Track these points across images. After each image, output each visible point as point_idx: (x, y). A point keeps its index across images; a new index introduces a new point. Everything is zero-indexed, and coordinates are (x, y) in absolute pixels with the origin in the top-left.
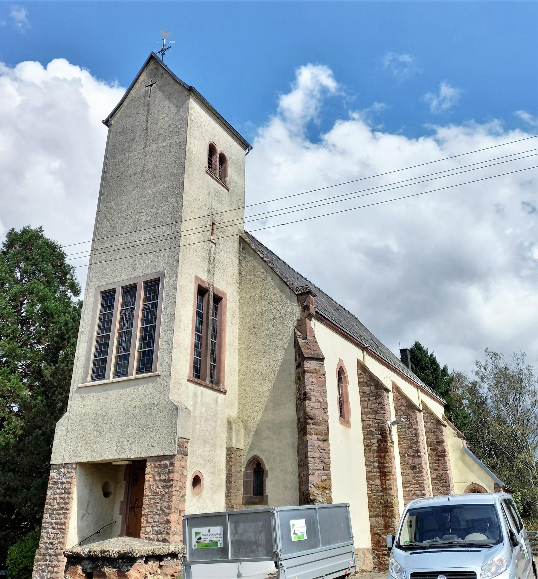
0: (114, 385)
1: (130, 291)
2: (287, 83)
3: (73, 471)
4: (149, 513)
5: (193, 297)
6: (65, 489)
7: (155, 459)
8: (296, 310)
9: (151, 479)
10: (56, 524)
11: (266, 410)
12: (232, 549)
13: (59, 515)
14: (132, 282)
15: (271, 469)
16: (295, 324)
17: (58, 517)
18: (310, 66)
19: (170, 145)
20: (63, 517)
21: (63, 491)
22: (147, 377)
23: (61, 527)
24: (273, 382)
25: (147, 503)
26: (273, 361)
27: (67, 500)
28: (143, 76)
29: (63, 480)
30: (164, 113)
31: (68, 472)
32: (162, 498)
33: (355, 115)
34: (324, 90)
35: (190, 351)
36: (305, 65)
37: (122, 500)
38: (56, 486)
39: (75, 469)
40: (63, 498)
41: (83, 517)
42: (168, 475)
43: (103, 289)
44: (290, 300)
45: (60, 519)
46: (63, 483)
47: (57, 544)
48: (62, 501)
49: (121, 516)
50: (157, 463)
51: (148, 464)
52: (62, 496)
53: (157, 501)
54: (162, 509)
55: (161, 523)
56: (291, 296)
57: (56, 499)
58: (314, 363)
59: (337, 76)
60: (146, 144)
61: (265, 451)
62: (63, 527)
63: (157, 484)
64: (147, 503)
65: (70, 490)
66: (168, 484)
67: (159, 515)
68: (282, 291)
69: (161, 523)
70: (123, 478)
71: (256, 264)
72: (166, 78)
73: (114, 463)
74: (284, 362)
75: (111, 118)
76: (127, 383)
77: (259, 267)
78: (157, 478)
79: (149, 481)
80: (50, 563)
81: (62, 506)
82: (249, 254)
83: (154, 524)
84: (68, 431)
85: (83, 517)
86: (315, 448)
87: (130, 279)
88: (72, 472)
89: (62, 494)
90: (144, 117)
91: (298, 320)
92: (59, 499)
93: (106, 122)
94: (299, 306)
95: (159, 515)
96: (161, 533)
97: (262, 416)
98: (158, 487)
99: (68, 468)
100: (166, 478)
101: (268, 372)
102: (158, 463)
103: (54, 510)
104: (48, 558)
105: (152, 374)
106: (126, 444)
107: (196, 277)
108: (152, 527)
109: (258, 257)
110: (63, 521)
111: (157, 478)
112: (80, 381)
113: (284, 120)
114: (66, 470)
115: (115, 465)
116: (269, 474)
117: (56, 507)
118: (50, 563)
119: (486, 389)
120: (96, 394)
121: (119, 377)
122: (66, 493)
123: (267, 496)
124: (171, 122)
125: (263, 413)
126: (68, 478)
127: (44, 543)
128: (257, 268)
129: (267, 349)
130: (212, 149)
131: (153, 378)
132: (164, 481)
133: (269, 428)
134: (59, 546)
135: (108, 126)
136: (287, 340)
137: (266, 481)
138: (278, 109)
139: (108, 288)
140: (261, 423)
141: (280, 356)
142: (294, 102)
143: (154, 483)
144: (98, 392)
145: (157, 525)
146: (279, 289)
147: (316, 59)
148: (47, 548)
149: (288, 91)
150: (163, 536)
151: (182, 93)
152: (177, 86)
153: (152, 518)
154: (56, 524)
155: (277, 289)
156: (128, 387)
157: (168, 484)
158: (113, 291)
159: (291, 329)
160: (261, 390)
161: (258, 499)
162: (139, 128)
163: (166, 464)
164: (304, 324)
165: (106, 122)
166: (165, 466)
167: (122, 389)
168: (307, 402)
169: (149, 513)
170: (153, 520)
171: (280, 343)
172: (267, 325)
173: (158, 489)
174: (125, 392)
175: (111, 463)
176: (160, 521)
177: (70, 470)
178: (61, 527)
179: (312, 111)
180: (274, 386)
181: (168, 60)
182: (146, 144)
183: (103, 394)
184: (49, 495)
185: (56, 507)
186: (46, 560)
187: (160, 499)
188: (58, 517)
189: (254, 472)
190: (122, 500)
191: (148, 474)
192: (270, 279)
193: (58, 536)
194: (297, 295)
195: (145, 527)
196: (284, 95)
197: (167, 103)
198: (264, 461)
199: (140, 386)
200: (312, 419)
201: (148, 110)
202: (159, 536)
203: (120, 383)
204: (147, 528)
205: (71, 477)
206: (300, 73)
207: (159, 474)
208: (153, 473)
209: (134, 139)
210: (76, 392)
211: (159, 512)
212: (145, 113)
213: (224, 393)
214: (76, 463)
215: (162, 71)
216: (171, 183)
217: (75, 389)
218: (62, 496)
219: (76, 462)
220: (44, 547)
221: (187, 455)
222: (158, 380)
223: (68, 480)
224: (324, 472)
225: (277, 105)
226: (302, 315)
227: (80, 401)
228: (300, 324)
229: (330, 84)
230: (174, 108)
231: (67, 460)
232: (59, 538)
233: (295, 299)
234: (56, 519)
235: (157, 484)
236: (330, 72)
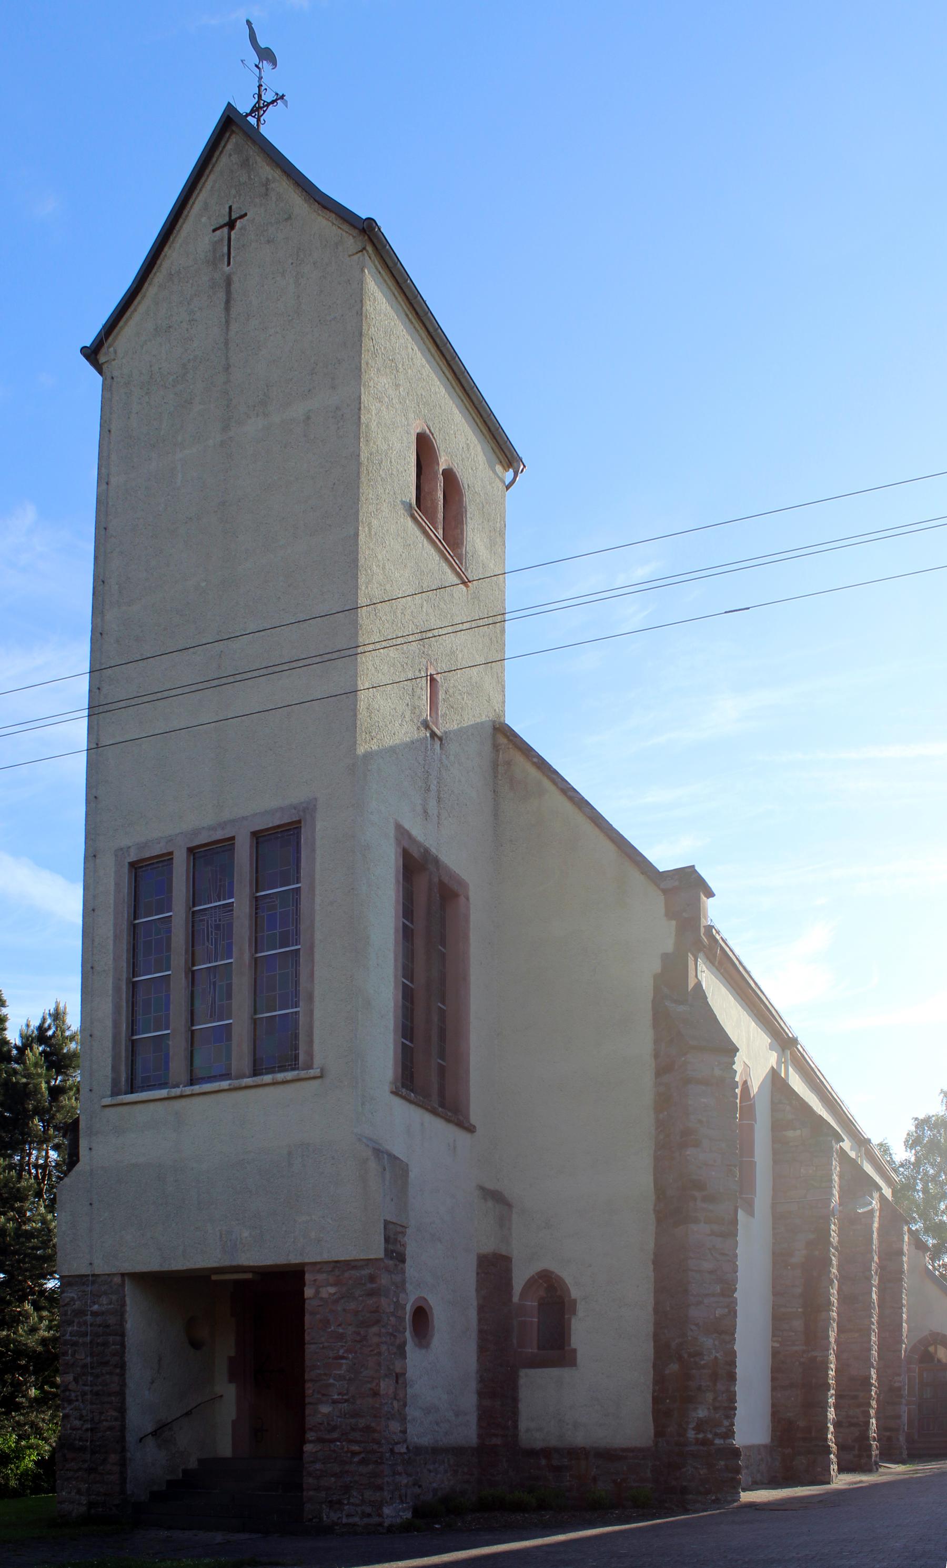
1: (210, 856)
5: (393, 880)
12: (647, 1526)
14: (219, 835)
35: (392, 1022)
41: (152, 1382)
51: (308, 1277)
73: (214, 1277)
85: (152, 1382)
87: (213, 828)
91: (665, 957)
93: (92, 354)
107: (399, 828)
115: (215, 1281)
116: (581, 1308)
119: (46, 1334)
123: (575, 1351)
130: (425, 448)
135: (99, 368)
137: (573, 1321)
158: (166, 859)
165: (92, 354)
168: (690, 1151)
181: (272, 127)
189: (540, 1305)
194: (664, 891)
213: (471, 1129)
214: (123, 1275)
219: (123, 1271)
221: (403, 1261)
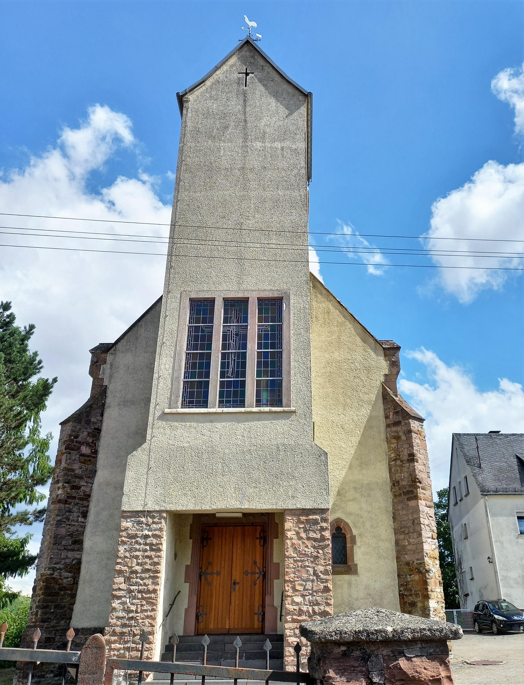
0: (224, 416)
2: (78, 119)
3: (163, 521)
4: (296, 579)
6: (151, 545)
7: (297, 512)
8: (382, 365)
9: (295, 537)
10: (139, 592)
11: (350, 467)
13: (142, 579)
15: (360, 535)
16: (382, 379)
17: (141, 582)
18: (107, 109)
19: (282, 149)
20: (150, 583)
21: (148, 548)
22: (254, 412)
23: (148, 595)
24: (358, 439)
25: (291, 566)
26: (357, 415)
27: (156, 560)
28: (233, 60)
29: (146, 532)
30: (268, 110)
31: (153, 523)
32: (315, 560)
33: (145, 177)
34: (117, 139)
36: (102, 106)
37: (189, 563)
38: (133, 541)
39: (165, 518)
40: (150, 557)
42: (320, 533)
43: (194, 295)
44: (375, 352)
45: (145, 584)
46: (146, 537)
47: (143, 619)
48: (147, 560)
49: (188, 585)
50: (303, 518)
52: (146, 554)
53: (307, 564)
54: (315, 574)
55: (316, 592)
56: (376, 348)
57: (137, 557)
58: (417, 423)
59: (135, 131)
60: (245, 140)
61: (351, 514)
62: (153, 595)
63: (303, 543)
64: (291, 566)
65: (160, 546)
66: (321, 544)
67: (313, 581)
68: (364, 341)
69: (316, 592)
70: (188, 535)
71: (330, 306)
72: (268, 72)
73: (217, 515)
74: (371, 418)
75: (190, 91)
76: (245, 416)
77: (334, 311)
78: (303, 535)
79: (291, 539)
80: (134, 645)
81: (148, 567)
82: (321, 294)
83: (305, 593)
84: (149, 469)
86: (424, 514)
87: (235, 291)
88: (161, 523)
89: (145, 551)
90: (239, 107)
91: (386, 375)
92: (141, 557)
94: (386, 361)
95: (313, 581)
96: (318, 604)
97: (346, 475)
98: (307, 547)
99: (153, 517)
100: (318, 536)
101: (352, 426)
102: (304, 518)
103: (133, 572)
104: (127, 638)
105: (242, 410)
106: (251, 491)
108: (303, 596)
109: (334, 300)
110: (151, 587)
111: (303, 535)
112: (166, 405)
113: (65, 155)
114: (150, 520)
117: (138, 568)
118: (134, 645)
120: (194, 424)
121: (237, 407)
122: (152, 550)
124: (281, 123)
125: (347, 472)
126: (155, 530)
127: (118, 618)
128: (332, 311)
129: (348, 401)
131: (285, 414)
132: (315, 540)
133: (355, 489)
134: (147, 621)
136: (373, 394)
138: (59, 141)
139: (202, 295)
140: (344, 483)
141: (365, 411)
142: (80, 141)
143: (300, 542)
144: (196, 422)
145: (310, 594)
146: (361, 339)
147: (116, 105)
148: (124, 626)
149: (75, 126)
150: (322, 608)
151: (293, 96)
152: (286, 86)
153: (301, 585)
154: (139, 592)
155: (358, 339)
156: (247, 420)
157: (321, 544)
159: (378, 383)
160: (344, 446)
161: (341, 567)
162: (234, 117)
163: (316, 519)
164: (393, 380)
166: (316, 522)
167: (238, 422)
169: (296, 579)
170: (302, 588)
171: (366, 398)
172: (348, 375)
173: (307, 550)
174: (243, 426)
175: (214, 515)
176: (315, 589)
177: (156, 520)
178: (148, 595)
179: (100, 158)
180: (360, 443)
182: (245, 140)
183: (208, 425)
184: (122, 551)
185: (138, 568)
186: (126, 642)
187: (312, 562)
188: (141, 582)
190: (189, 563)
191: (289, 530)
192: (350, 326)
193: (145, 608)
195: (291, 596)
196: (68, 129)
197: (273, 102)
198: (351, 525)
199: (266, 422)
200: (420, 483)
201: (245, 101)
202: (316, 608)
203: (234, 415)
204: (294, 598)
205: (161, 530)
206: (94, 112)
207: (306, 531)
208: (297, 529)
209: (227, 127)
210: (160, 418)
211: (311, 578)
212: (241, 102)
214: (167, 511)
215: (261, 62)
216: (288, 192)
217: (158, 414)
218: (146, 554)
220: (119, 623)
222: (293, 417)
223: (155, 533)
224: (432, 540)
225: (59, 137)
226: (390, 370)
227: (168, 431)
228: (388, 380)
229: (127, 136)
230: (284, 109)
231: (151, 506)
232: (146, 611)
233: (382, 352)
234: (137, 584)
235: (303, 543)
236: (129, 123)
